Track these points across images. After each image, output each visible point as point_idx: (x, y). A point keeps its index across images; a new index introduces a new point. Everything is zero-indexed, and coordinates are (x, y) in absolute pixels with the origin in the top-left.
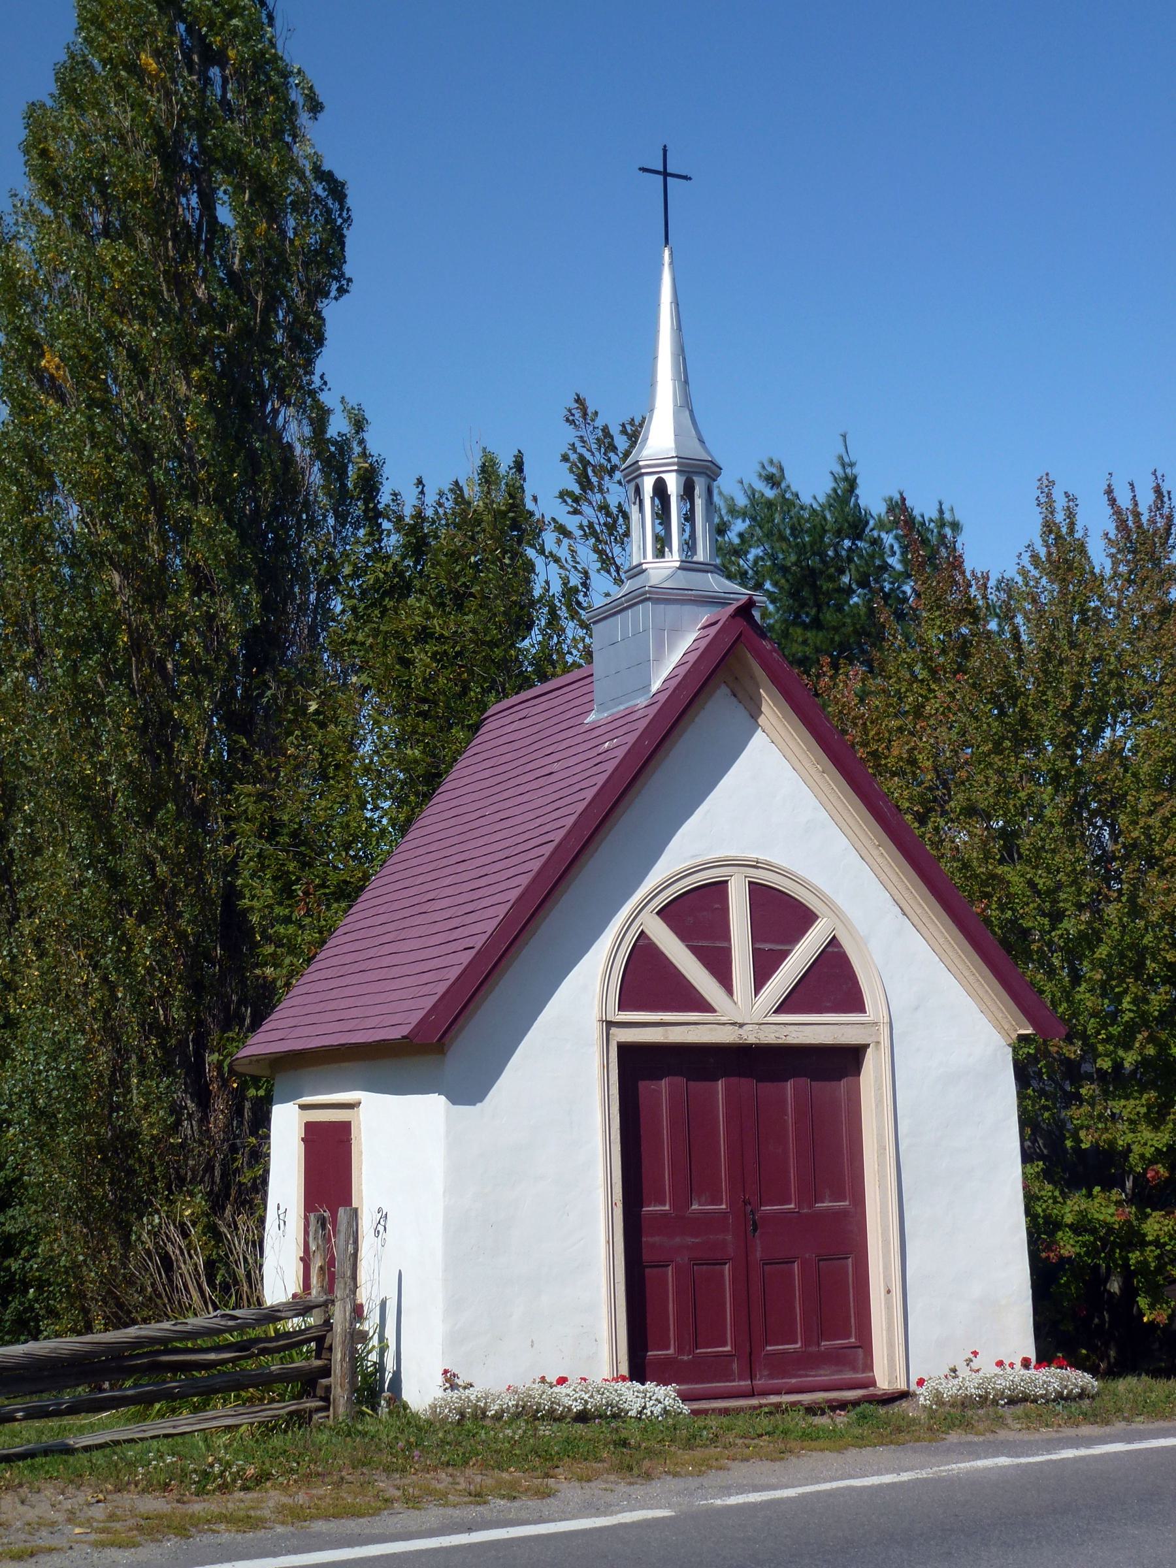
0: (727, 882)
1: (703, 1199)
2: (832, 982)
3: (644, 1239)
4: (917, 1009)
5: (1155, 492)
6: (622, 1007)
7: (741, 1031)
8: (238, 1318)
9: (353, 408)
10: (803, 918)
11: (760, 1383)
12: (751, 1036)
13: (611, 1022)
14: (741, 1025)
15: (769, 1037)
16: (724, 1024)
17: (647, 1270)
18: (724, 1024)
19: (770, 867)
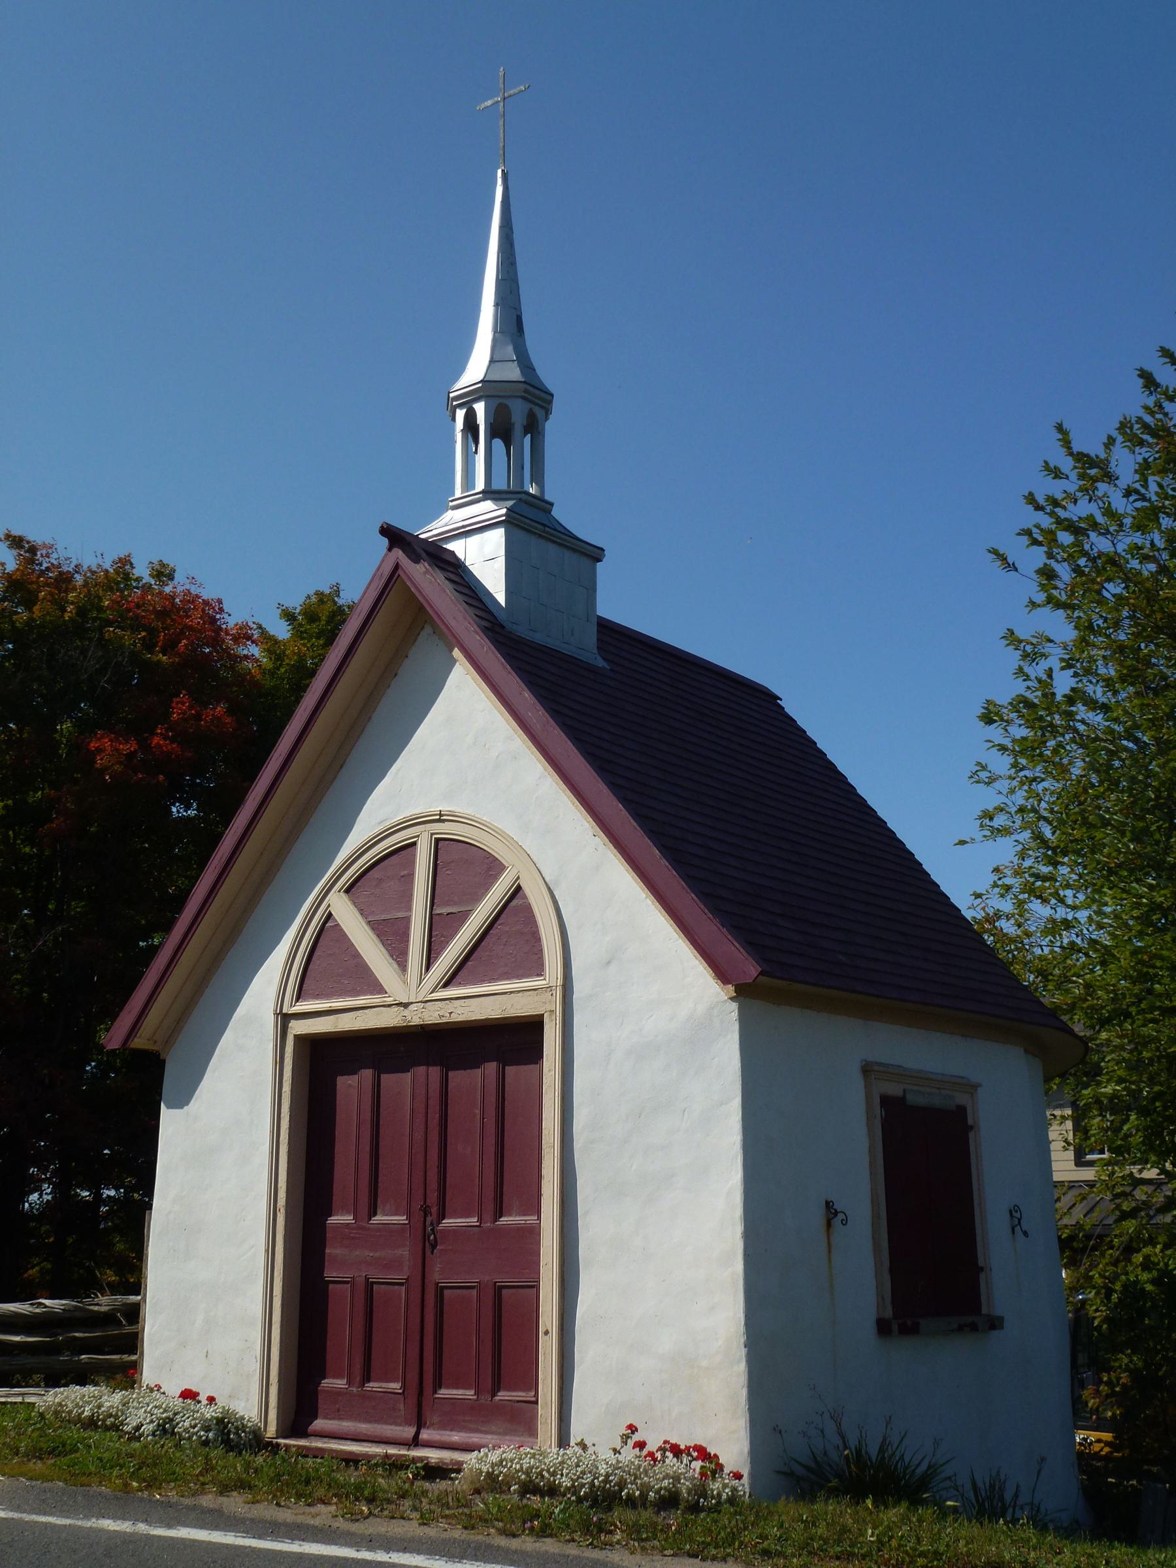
0: (414, 844)
1: (388, 1207)
2: (512, 939)
3: (327, 1251)
4: (609, 963)
5: (1140, 376)
6: (538, 969)
7: (406, 1012)
8: (46, 1307)
9: (1076, 675)
10: (492, 867)
11: (425, 1435)
12: (416, 1017)
13: (286, 1015)
14: (406, 1005)
15: (432, 1015)
16: (390, 1006)
17: (331, 1286)
18: (390, 1006)
19: (455, 818)
